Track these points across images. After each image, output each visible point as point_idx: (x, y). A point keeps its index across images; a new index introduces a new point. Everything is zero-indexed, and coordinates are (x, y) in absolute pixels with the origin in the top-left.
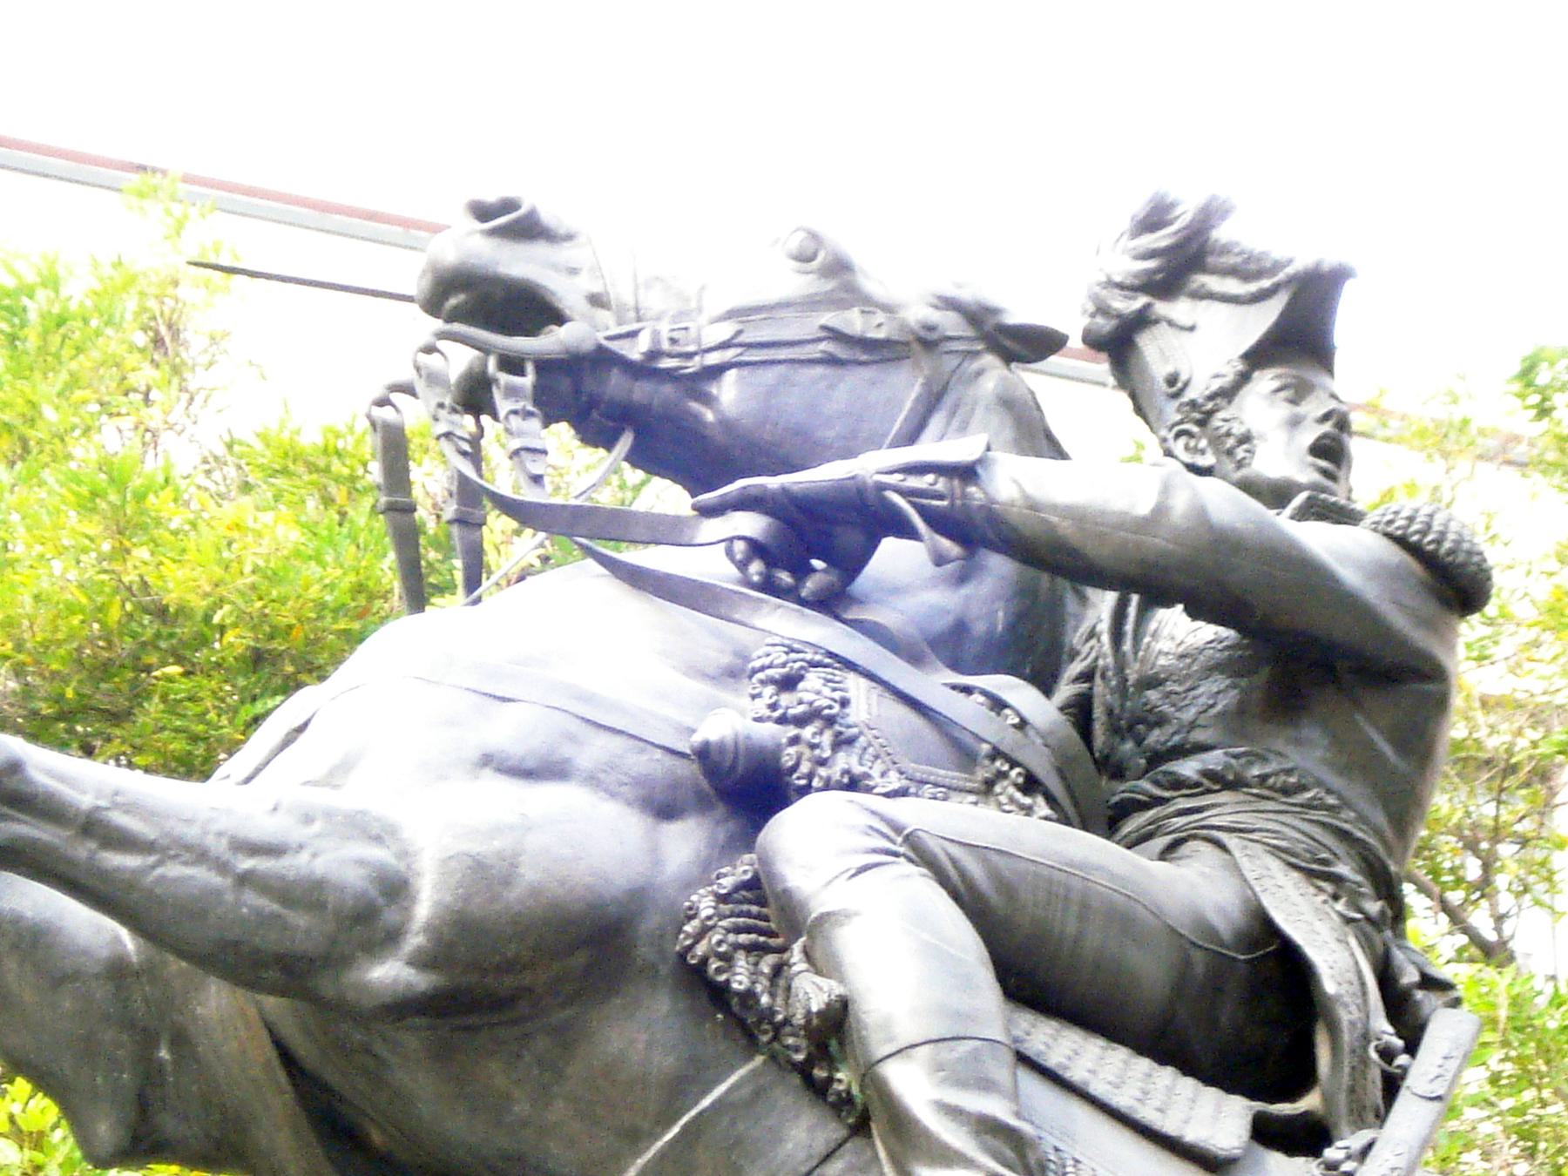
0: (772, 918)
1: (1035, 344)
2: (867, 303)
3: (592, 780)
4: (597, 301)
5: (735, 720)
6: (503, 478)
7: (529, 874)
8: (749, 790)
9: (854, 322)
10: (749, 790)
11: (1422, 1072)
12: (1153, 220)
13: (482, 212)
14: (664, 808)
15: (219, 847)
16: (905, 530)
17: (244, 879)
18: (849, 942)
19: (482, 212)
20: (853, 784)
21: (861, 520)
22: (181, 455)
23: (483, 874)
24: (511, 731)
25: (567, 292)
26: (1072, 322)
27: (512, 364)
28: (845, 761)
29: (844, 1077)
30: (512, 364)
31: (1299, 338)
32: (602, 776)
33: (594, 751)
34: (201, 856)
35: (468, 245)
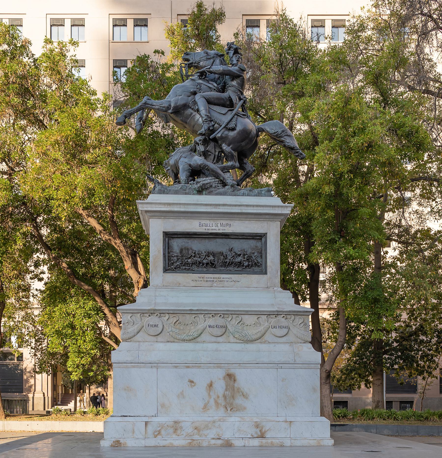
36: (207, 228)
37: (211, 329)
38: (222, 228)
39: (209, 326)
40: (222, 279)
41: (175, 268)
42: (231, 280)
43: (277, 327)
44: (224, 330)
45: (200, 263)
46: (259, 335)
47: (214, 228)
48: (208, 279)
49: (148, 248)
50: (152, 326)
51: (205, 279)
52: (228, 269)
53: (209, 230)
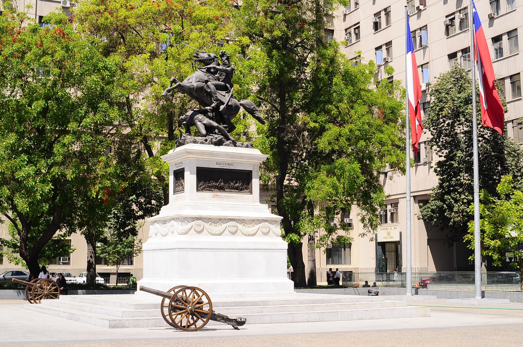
0: (208, 87)
10: (207, 82)
23: (197, 87)
24: (198, 80)
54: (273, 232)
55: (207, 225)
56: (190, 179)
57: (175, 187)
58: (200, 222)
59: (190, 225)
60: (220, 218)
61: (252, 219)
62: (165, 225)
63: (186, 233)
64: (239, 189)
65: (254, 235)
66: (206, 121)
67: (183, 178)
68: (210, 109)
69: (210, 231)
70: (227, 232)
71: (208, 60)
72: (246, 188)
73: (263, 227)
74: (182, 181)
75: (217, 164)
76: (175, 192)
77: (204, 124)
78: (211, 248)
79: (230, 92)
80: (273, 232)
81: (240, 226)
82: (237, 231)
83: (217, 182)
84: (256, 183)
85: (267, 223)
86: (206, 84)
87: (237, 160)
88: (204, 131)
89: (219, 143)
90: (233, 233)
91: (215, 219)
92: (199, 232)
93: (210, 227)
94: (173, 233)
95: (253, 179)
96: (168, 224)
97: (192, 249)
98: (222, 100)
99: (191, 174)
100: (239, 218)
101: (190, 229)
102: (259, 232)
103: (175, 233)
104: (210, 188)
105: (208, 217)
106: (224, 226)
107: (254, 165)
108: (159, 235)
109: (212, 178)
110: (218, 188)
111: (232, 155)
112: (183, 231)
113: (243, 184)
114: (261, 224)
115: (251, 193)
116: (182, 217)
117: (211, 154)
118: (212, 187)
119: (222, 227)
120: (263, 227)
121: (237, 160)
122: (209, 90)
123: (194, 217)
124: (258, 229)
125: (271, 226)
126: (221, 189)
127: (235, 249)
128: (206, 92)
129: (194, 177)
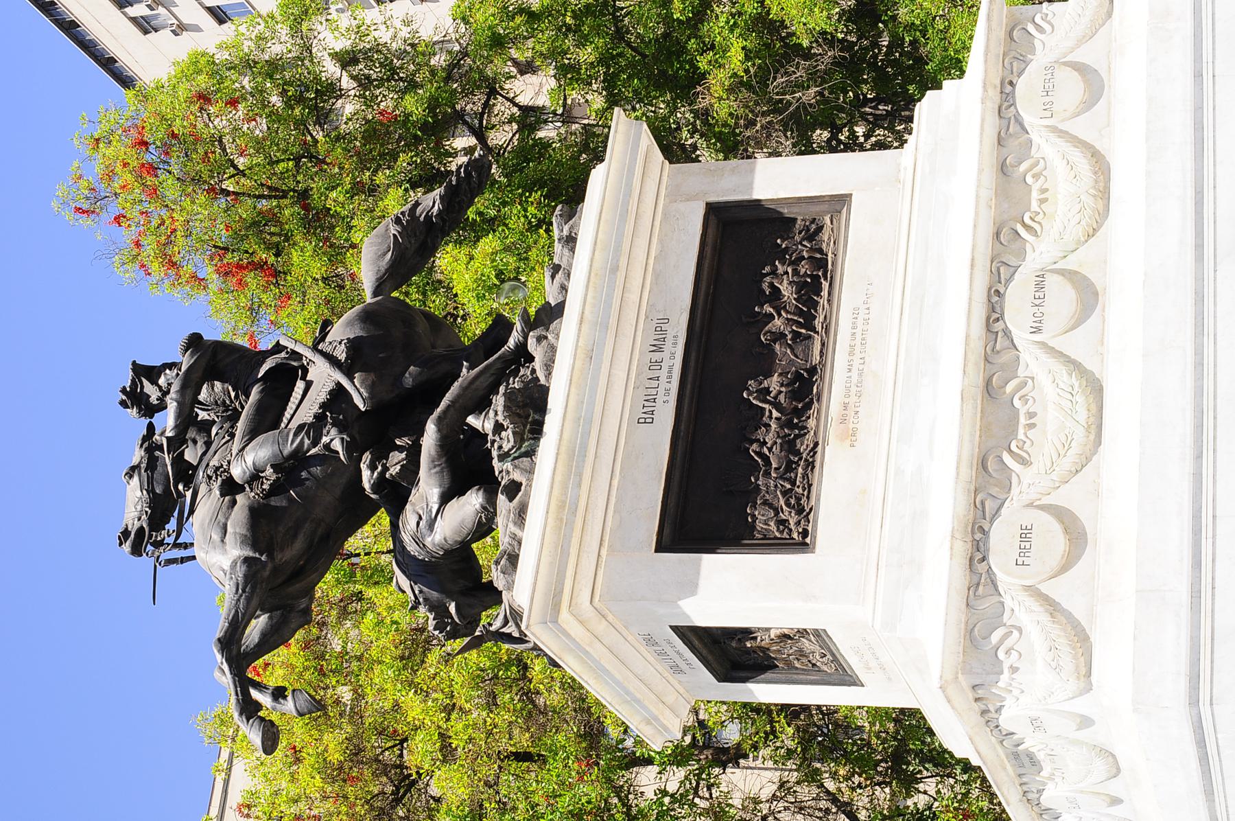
0: (255, 476)
1: (151, 428)
2: (140, 462)
3: (227, 519)
4: (139, 519)
5: (216, 486)
6: (170, 540)
7: (244, 532)
8: (230, 488)
9: (143, 466)
10: (230, 488)
11: (291, 345)
12: (123, 404)
13: (121, 544)
14: (234, 502)
15: (237, 597)
16: (182, 453)
17: (244, 591)
18: (260, 463)
19: (121, 544)
20: (229, 462)
21: (179, 461)
22: (369, 298)
23: (244, 541)
24: (216, 537)
25: (137, 524)
26: (145, 421)
27: (150, 536)
28: (225, 464)
29: (304, 27)
30: (150, 536)
31: (151, 373)
32: (514, 70)
33: (221, 518)
34: (239, 600)
35: (127, 547)
36: (660, 398)
37: (1045, 327)
38: (668, 347)
39: (1037, 330)
40: (858, 341)
41: (800, 511)
42: (862, 311)
43: (1047, 99)
44: (1052, 281)
45: (789, 424)
46: (1077, 156)
47: (663, 374)
48: (854, 389)
49: (607, 137)
50: (1023, 552)
51: (853, 399)
52: (819, 328)
53: (668, 391)
54: (1081, 41)
55: (1028, 483)
56: (733, 588)
57: (813, 674)
58: (1002, 537)
59: (1021, 611)
60: (978, 393)
61: (990, 177)
62: (1040, 756)
63: (1081, 638)
64: (817, 278)
65: (1100, 165)
66: (427, 489)
67: (746, 633)
68: (372, 468)
69: (1067, 463)
70: (1075, 345)
71: (150, 481)
72: (813, 233)
73: (1048, 108)
74: (763, 640)
75: (647, 418)
76: (845, 677)
77: (445, 499)
78: (1189, 454)
79: (295, 355)
80: (1081, 41)
81: (1039, 253)
82: (1071, 276)
83: (756, 418)
84: (778, 178)
85: (1021, 84)
86: (241, 489)
87: (633, 297)
88: (473, 500)
89: (530, 408)
90: (1088, 296)
91: (985, 429)
92: (1076, 536)
93: (1040, 461)
94: (1085, 722)
95: (756, 196)
96: (1032, 743)
97: (1196, 594)
98: (323, 397)
99: (691, 587)
100: (983, 263)
101: (1052, 607)
102: (1081, 128)
103: (1082, 706)
104: (799, 460)
105: (967, 473)
106: (1032, 362)
107: (676, 195)
108: (1114, 787)
109: (734, 463)
110: (801, 413)
111: (602, 324)
112: (1067, 662)
113: (781, 254)
114: (1027, 119)
115: (840, 202)
116: (966, 668)
117: (575, 457)
118: (790, 446)
119: (1043, 380)
120: (1048, 108)
121: (633, 297)
122: (269, 471)
123: (961, 578)
124: (1062, 134)
125: (1039, 61)
126: (805, 388)
127: (1199, 279)
128: (276, 489)
129: (718, 568)
